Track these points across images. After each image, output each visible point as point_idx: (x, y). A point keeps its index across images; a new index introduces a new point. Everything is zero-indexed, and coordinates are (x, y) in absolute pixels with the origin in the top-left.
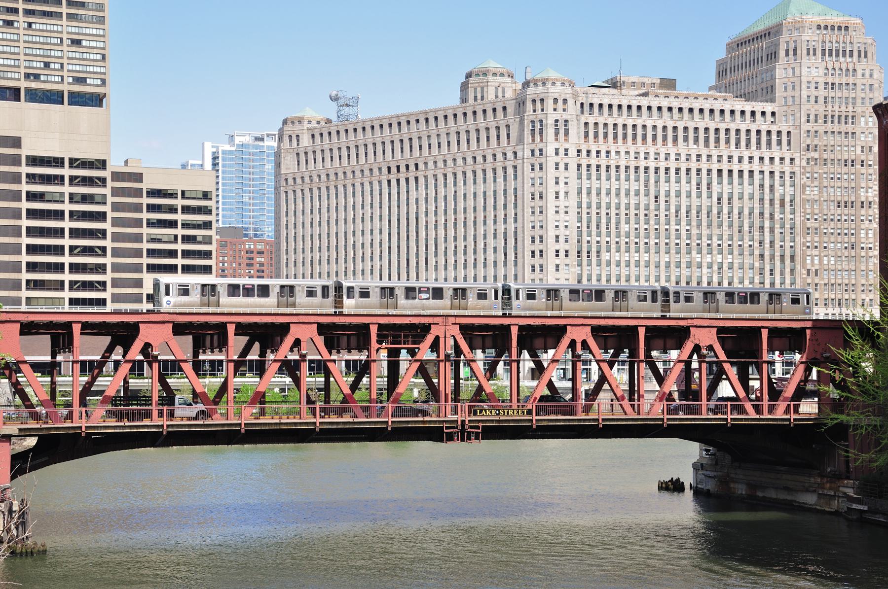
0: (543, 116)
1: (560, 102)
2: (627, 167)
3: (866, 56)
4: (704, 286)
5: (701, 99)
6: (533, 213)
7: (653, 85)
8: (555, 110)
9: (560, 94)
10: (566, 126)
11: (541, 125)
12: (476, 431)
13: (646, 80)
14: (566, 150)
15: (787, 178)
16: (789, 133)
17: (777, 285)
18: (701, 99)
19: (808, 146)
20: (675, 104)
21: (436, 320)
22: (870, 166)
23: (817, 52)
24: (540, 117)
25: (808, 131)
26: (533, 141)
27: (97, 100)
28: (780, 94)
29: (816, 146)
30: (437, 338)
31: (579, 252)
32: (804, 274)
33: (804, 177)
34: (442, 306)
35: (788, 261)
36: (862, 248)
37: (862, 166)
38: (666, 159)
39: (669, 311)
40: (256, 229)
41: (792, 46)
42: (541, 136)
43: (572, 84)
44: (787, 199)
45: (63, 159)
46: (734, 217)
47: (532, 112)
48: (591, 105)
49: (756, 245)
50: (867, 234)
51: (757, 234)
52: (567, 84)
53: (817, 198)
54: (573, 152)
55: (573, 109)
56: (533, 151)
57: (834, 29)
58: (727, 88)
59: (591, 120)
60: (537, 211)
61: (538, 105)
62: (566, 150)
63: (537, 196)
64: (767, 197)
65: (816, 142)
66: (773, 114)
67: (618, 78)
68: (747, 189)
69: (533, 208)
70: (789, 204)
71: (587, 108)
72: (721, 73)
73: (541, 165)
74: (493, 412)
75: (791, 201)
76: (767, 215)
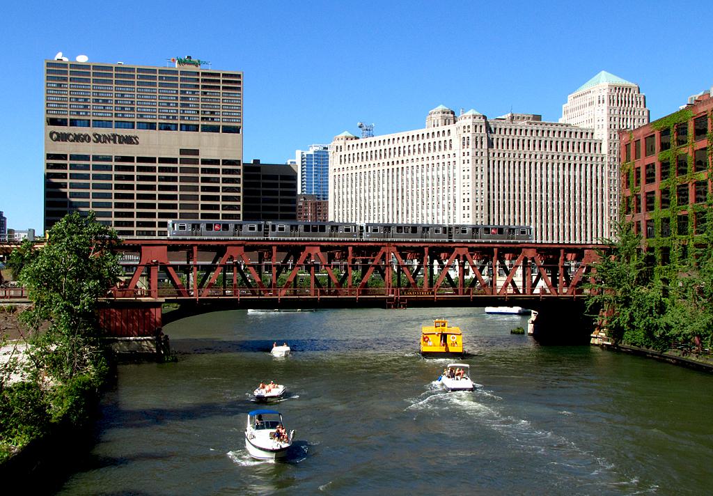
5: (554, 126)
9: (479, 123)
27: (236, 130)
40: (324, 195)
45: (219, 160)
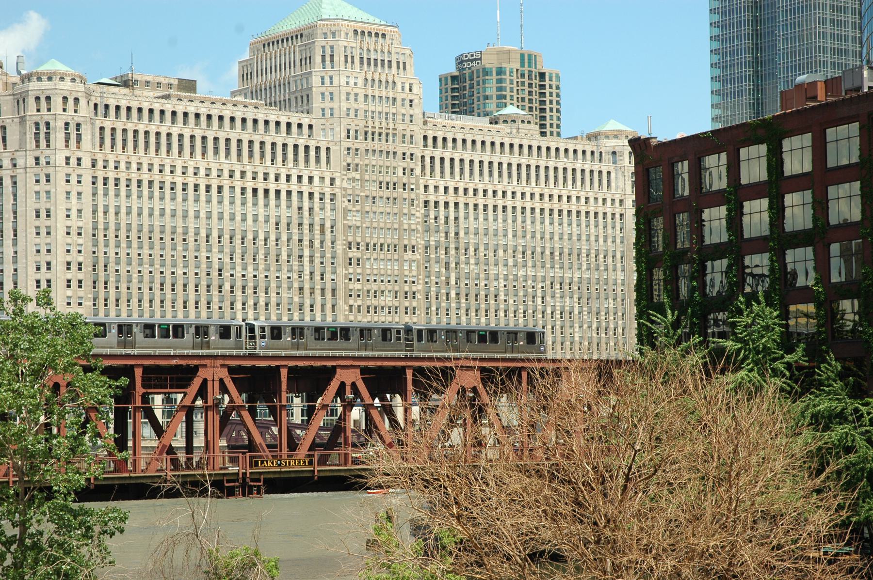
0: (50, 117)
1: (71, 102)
2: (596, 214)
3: (404, 68)
4: (492, 325)
5: (219, 105)
6: (38, 234)
7: (170, 85)
8: (64, 110)
10: (78, 130)
11: (48, 128)
12: (258, 484)
13: (162, 80)
14: (79, 159)
15: (327, 200)
16: (328, 149)
17: (318, 319)
18: (219, 105)
19: (349, 165)
20: (192, 109)
21: (203, 362)
22: (412, 190)
23: (355, 60)
24: (46, 118)
25: (349, 149)
26: (38, 146)
28: (317, 105)
29: (357, 165)
30: (205, 381)
31: (94, 282)
32: (346, 310)
33: (345, 200)
34: (218, 347)
35: (329, 295)
36: (406, 282)
37: (404, 189)
38: (195, 174)
39: (413, 351)
41: (328, 52)
42: (48, 141)
43: (83, 81)
44: (328, 225)
46: (237, 242)
47: (35, 113)
48: (107, 107)
49: (296, 276)
50: (410, 266)
51: (295, 263)
52: (78, 80)
53: (358, 224)
54: (86, 162)
55: (85, 110)
56: (37, 159)
57: (371, 36)
58: (254, 93)
59: (108, 124)
60: (43, 231)
61: (43, 103)
62: (79, 159)
63: (43, 214)
64: (306, 222)
65: (357, 161)
66: (310, 127)
67: (130, 75)
68: (284, 212)
69: (37, 228)
70: (330, 230)
71: (101, 109)
72: (245, 76)
73: (48, 176)
74: (275, 463)
75: (332, 227)
76: (306, 242)
